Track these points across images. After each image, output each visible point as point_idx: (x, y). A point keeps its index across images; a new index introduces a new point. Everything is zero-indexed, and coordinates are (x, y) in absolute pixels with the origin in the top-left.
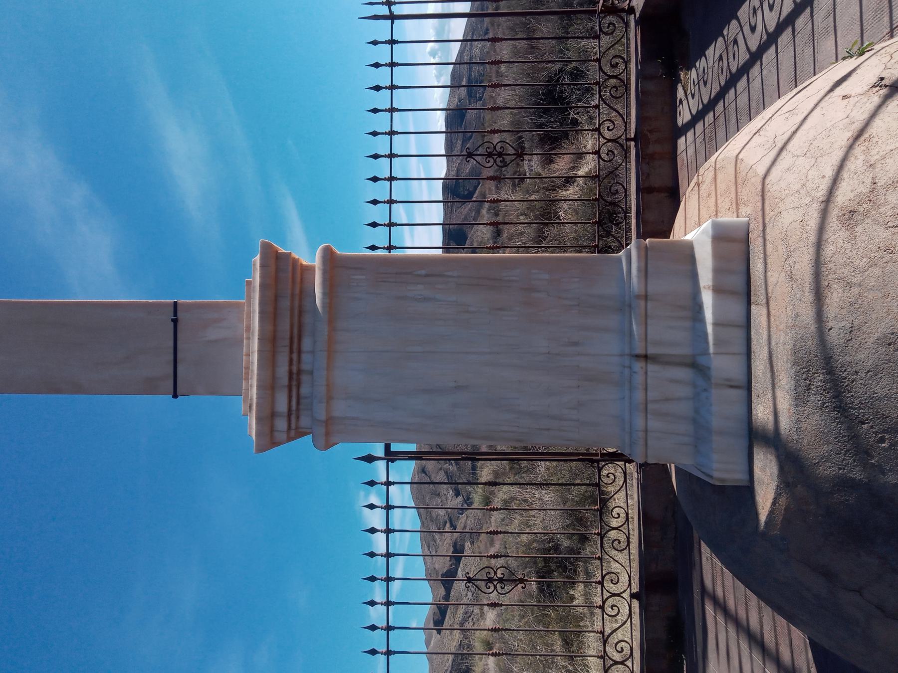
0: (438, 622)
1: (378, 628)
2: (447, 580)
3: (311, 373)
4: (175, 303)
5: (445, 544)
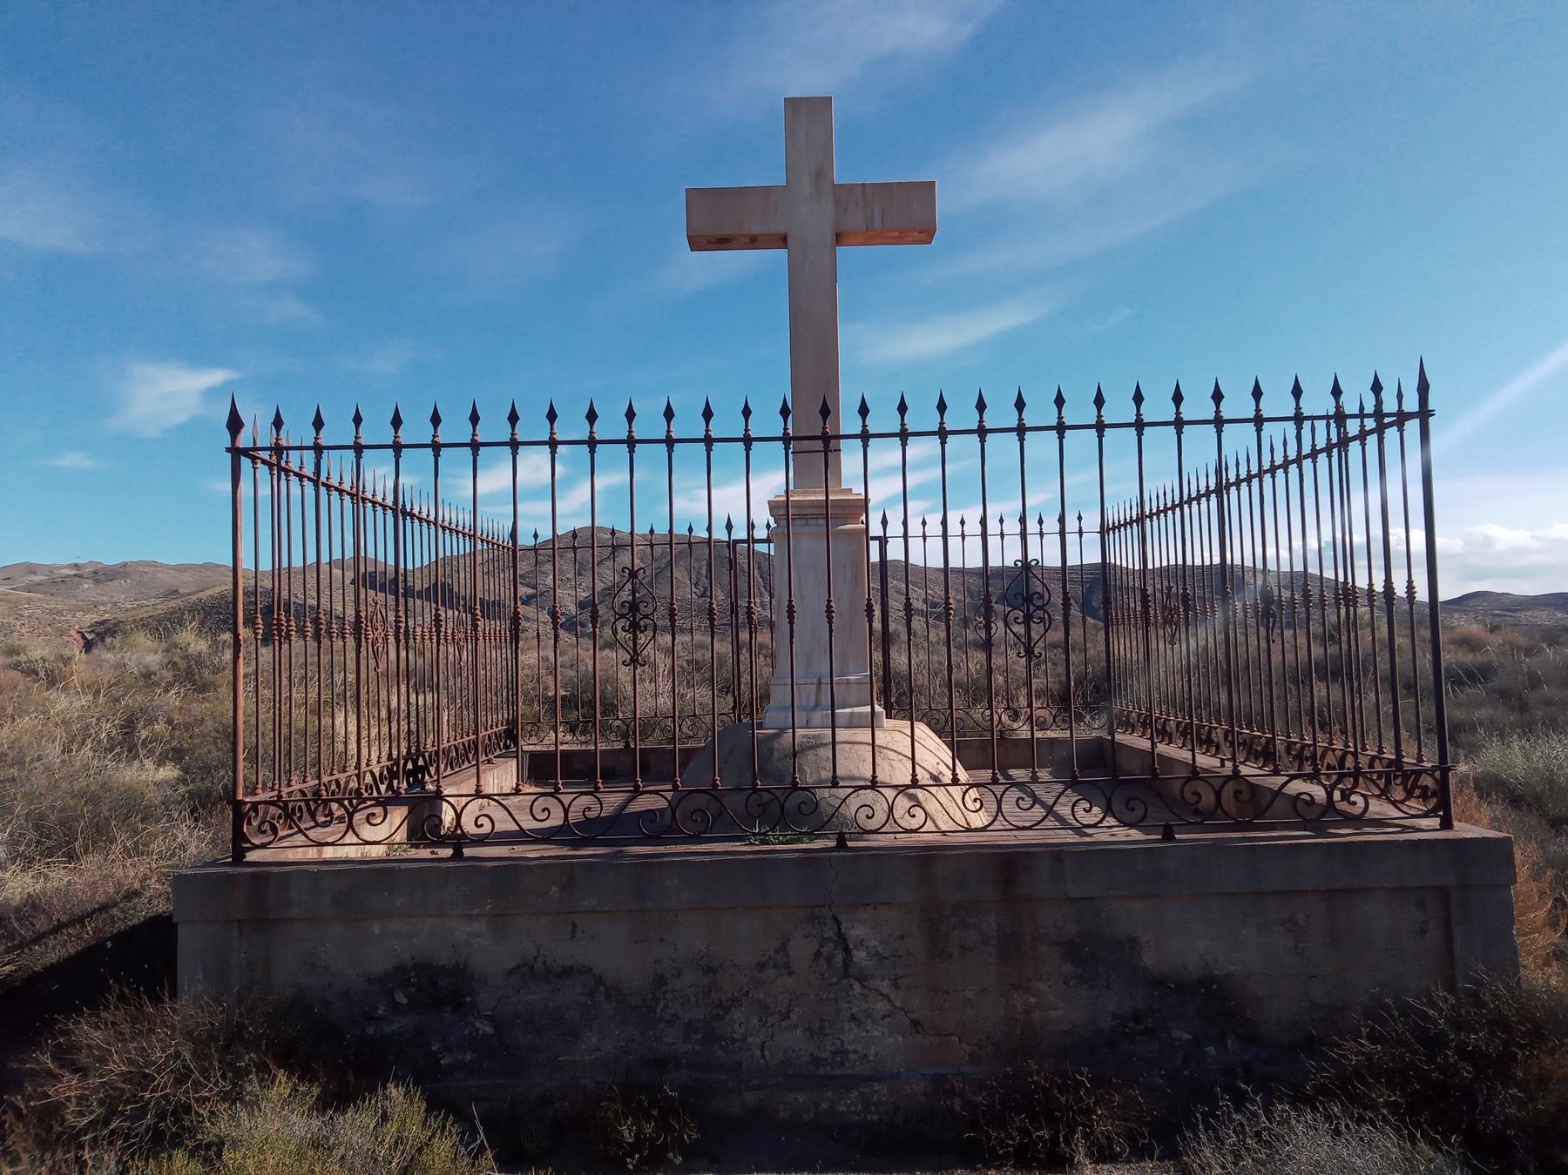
0: (367, 579)
1: (318, 432)
2: (440, 593)
3: (807, 525)
4: (840, 450)
5: (494, 587)
